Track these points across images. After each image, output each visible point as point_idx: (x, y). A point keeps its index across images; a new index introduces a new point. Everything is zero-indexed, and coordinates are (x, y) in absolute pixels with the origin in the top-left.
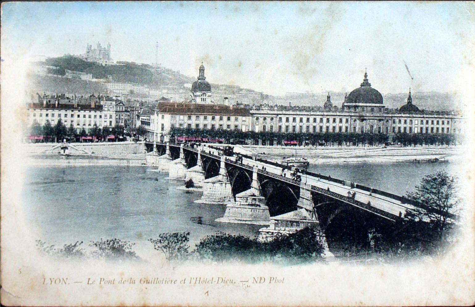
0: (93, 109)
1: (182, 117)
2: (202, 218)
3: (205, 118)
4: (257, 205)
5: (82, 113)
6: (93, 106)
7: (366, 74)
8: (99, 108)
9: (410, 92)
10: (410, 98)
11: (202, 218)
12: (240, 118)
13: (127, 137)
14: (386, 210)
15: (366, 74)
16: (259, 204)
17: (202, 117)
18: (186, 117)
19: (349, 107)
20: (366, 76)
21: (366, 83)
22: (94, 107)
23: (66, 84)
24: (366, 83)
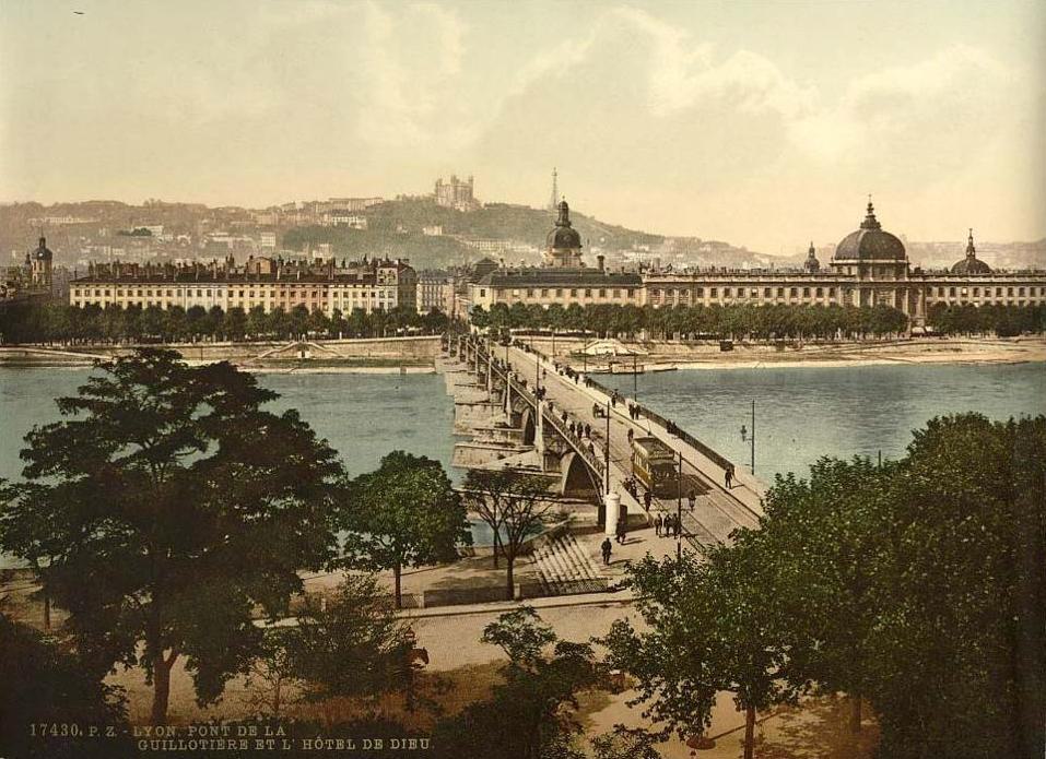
0: (360, 282)
1: (516, 292)
2: (440, 180)
3: (574, 295)
4: (510, 444)
5: (341, 290)
6: (360, 277)
7: (870, 205)
8: (370, 280)
9: (971, 238)
10: (971, 249)
11: (440, 180)
12: (508, 291)
13: (336, 479)
14: (691, 448)
15: (870, 205)
16: (512, 441)
17: (567, 292)
18: (524, 292)
19: (840, 266)
20: (870, 209)
21: (871, 224)
22: (269, 272)
23: (671, 530)
24: (871, 224)
